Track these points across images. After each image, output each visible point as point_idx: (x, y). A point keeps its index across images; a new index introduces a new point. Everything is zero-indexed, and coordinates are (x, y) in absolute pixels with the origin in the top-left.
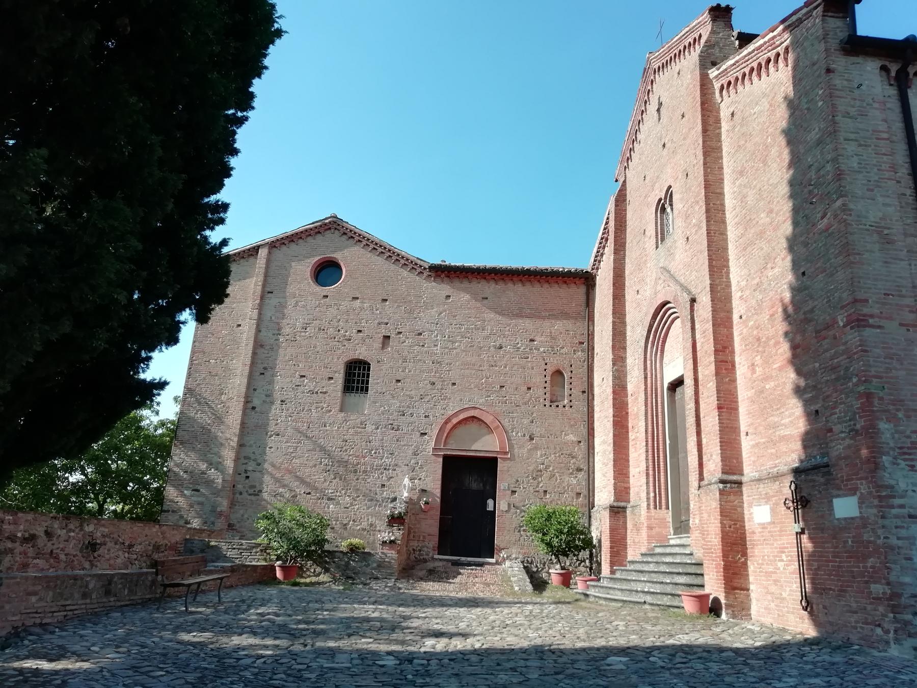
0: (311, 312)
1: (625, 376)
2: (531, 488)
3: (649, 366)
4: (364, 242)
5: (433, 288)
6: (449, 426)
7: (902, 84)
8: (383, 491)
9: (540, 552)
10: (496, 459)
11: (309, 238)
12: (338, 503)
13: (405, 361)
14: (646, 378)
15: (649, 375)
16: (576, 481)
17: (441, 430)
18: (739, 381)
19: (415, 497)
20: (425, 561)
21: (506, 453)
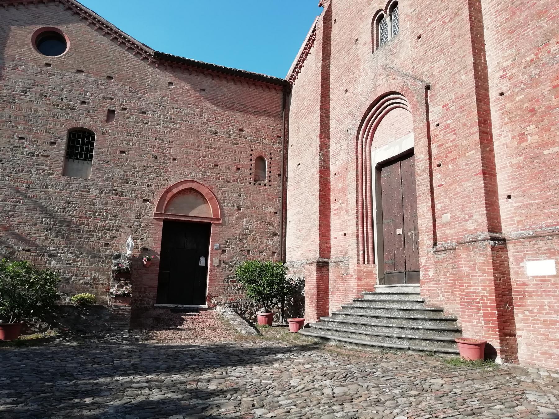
0: (33, 77)
1: (329, 160)
2: (238, 248)
3: (359, 149)
4: (90, 21)
6: (170, 195)
8: (107, 249)
10: (210, 224)
11: (31, 6)
12: (60, 260)
13: (129, 134)
14: (357, 159)
15: (360, 157)
16: (272, 243)
18: (496, 152)
19: (137, 255)
21: (219, 220)
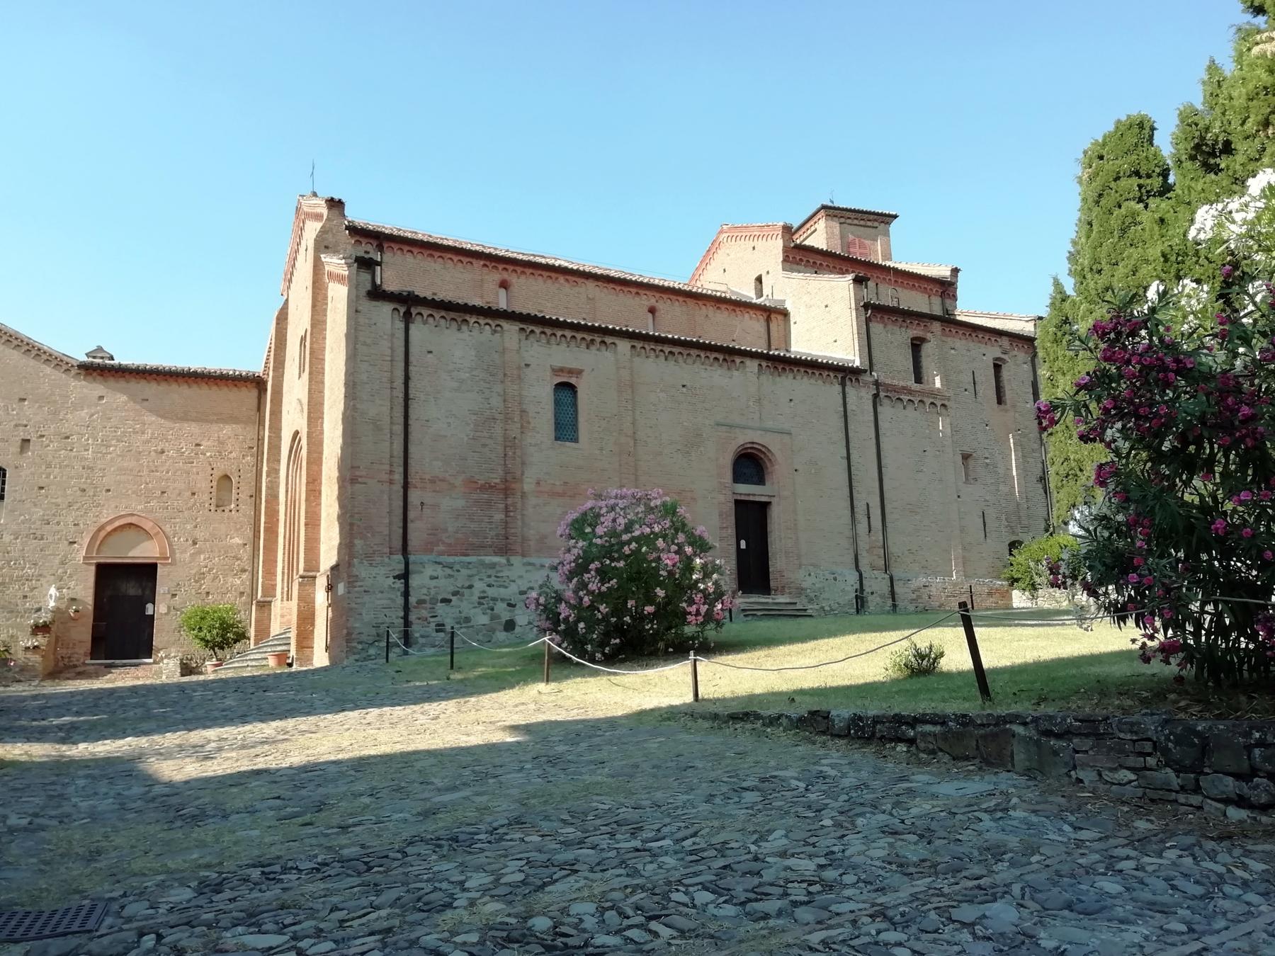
5: (82, 387)
6: (103, 534)
7: (408, 318)
9: (197, 649)
17: (93, 538)
19: (63, 607)
20: (75, 666)
